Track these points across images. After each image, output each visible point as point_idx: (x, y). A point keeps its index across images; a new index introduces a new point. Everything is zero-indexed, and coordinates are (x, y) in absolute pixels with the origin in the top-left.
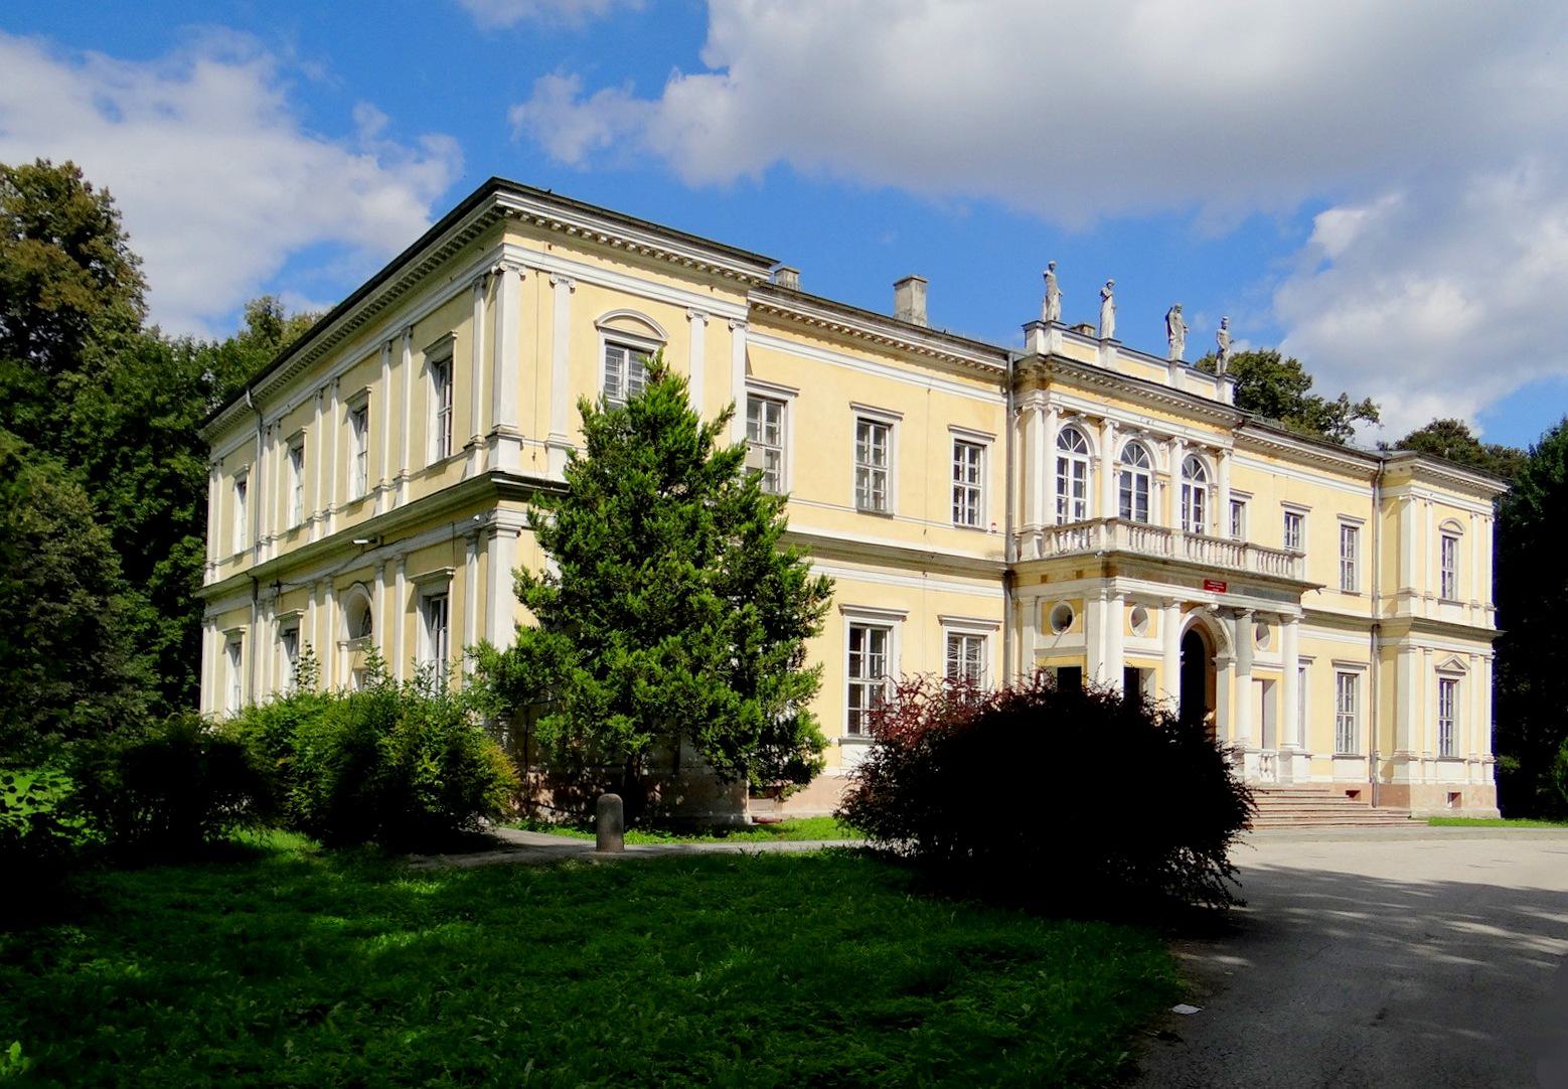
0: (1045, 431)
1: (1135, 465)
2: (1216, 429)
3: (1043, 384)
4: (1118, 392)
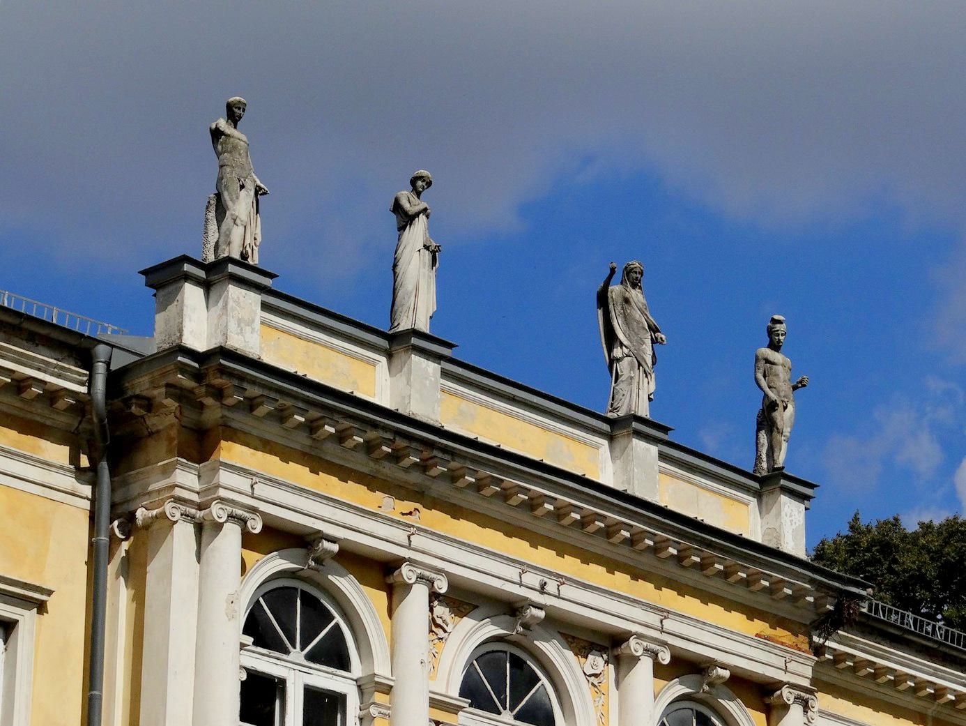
0: (204, 595)
1: (297, 655)
2: (759, 626)
3: (199, 446)
4: (441, 489)
